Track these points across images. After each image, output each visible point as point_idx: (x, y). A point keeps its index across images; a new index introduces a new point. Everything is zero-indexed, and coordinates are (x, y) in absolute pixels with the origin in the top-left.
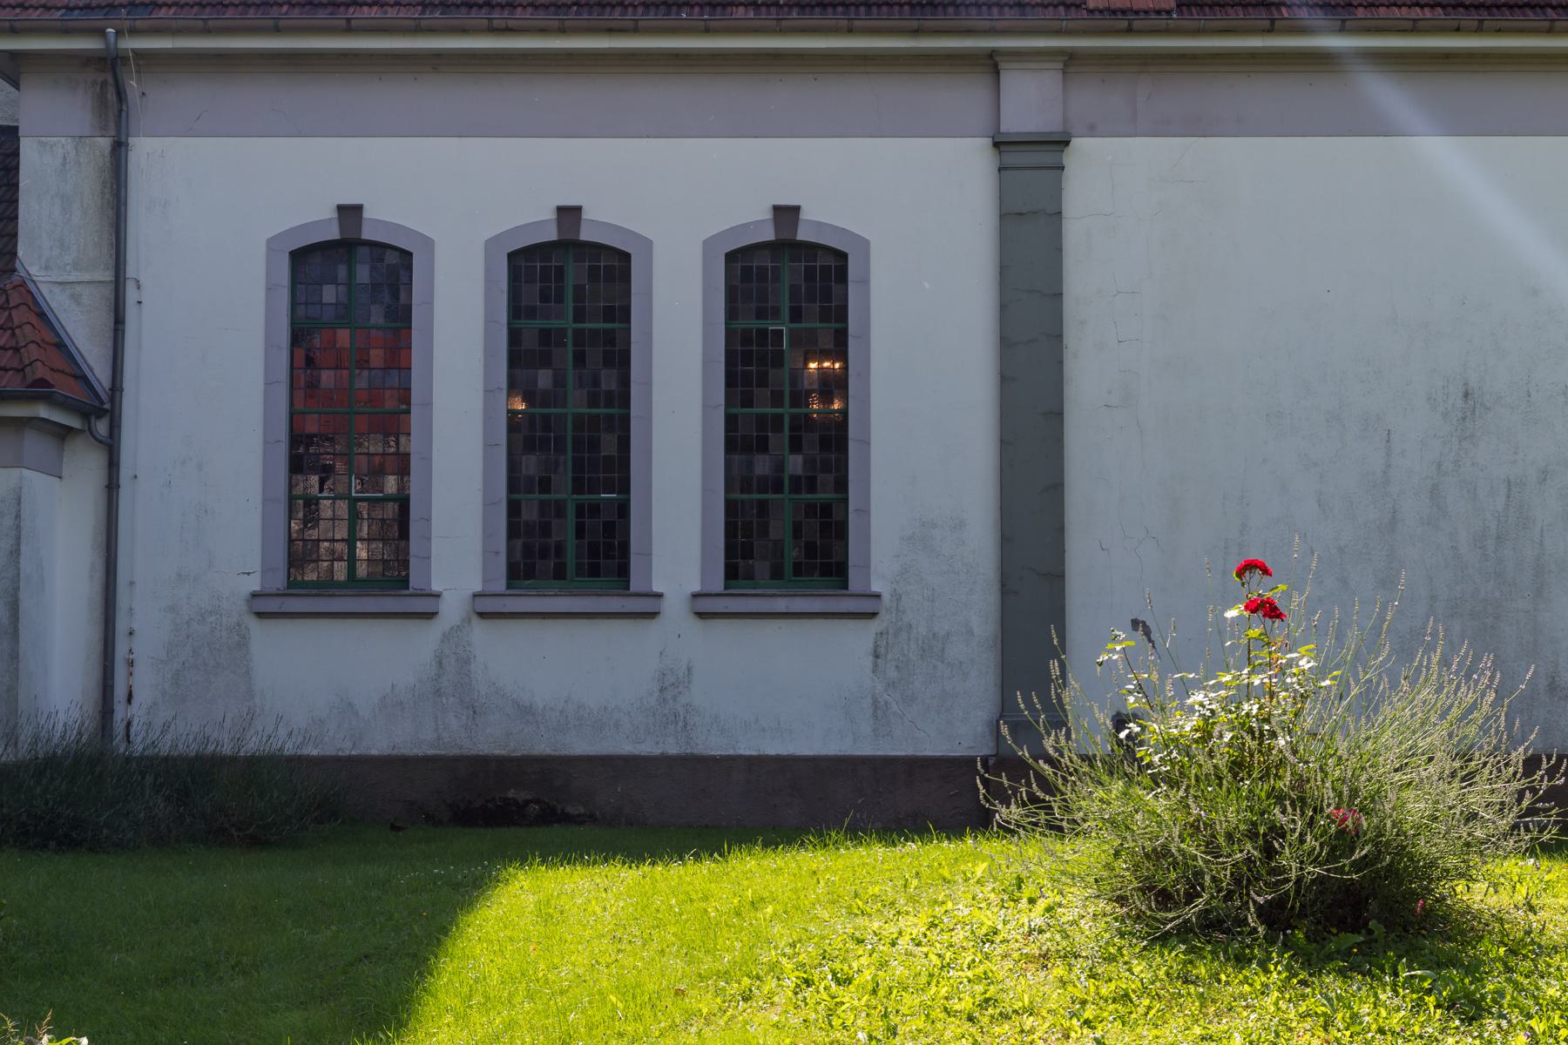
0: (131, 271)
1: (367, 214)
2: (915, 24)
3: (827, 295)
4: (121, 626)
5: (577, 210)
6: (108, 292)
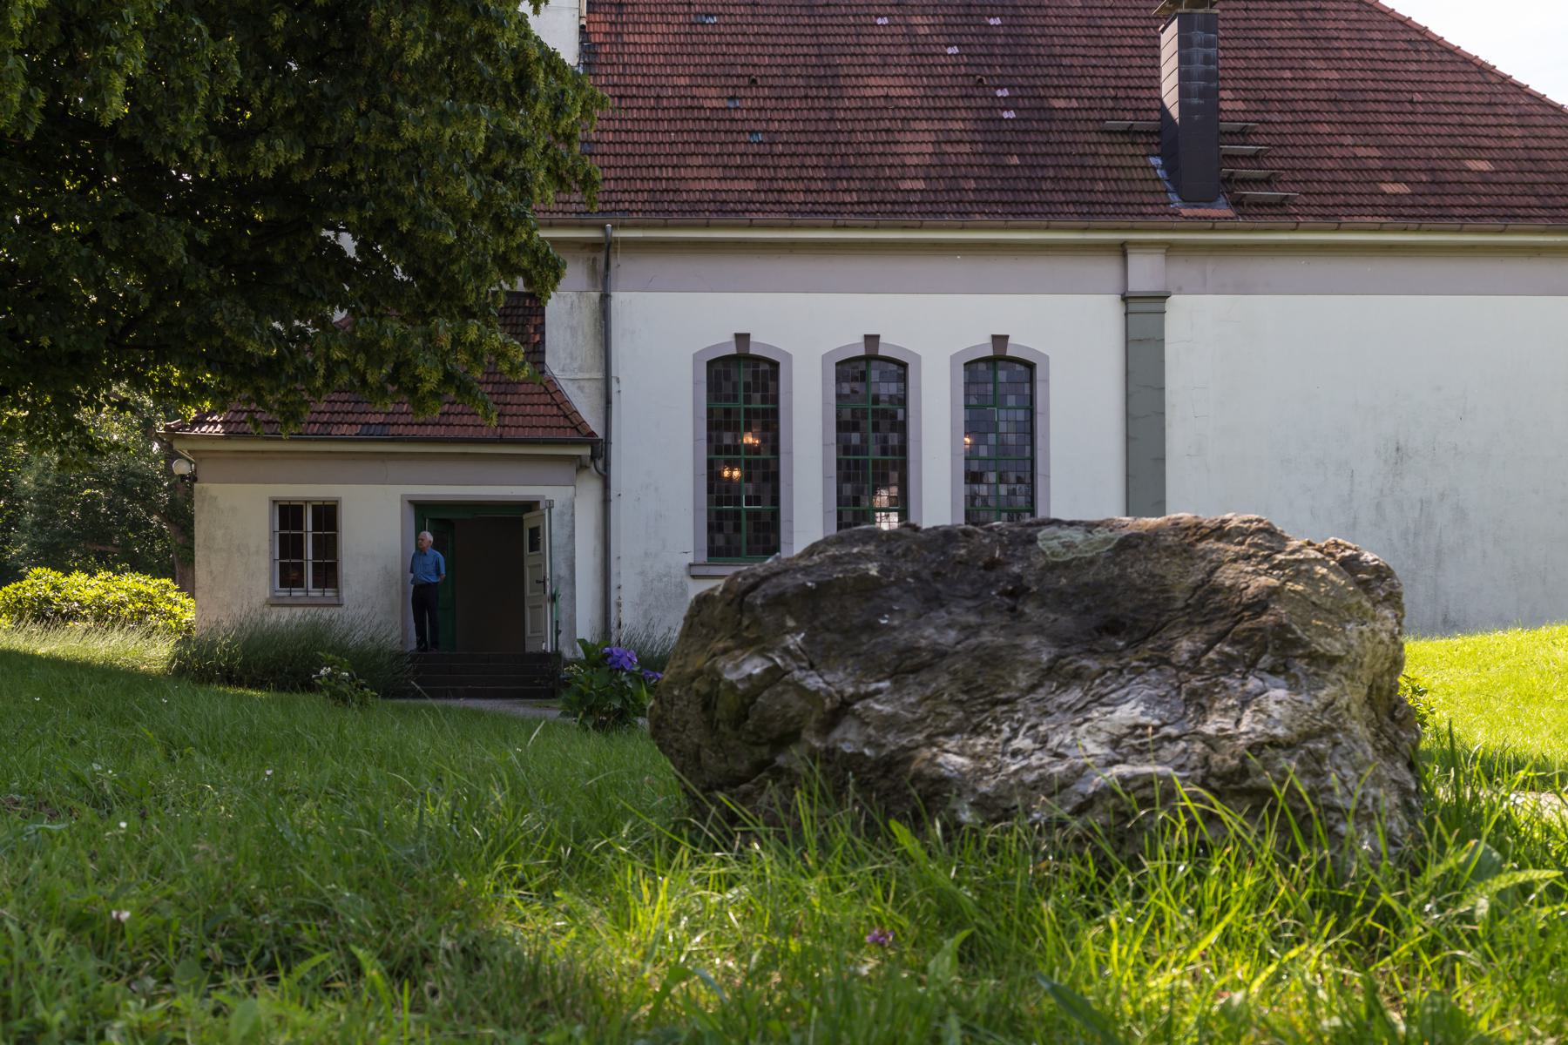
0: (614, 374)
1: (752, 339)
2: (1086, 224)
3: (765, 388)
4: (614, 584)
5: (747, 336)
6: (601, 385)
